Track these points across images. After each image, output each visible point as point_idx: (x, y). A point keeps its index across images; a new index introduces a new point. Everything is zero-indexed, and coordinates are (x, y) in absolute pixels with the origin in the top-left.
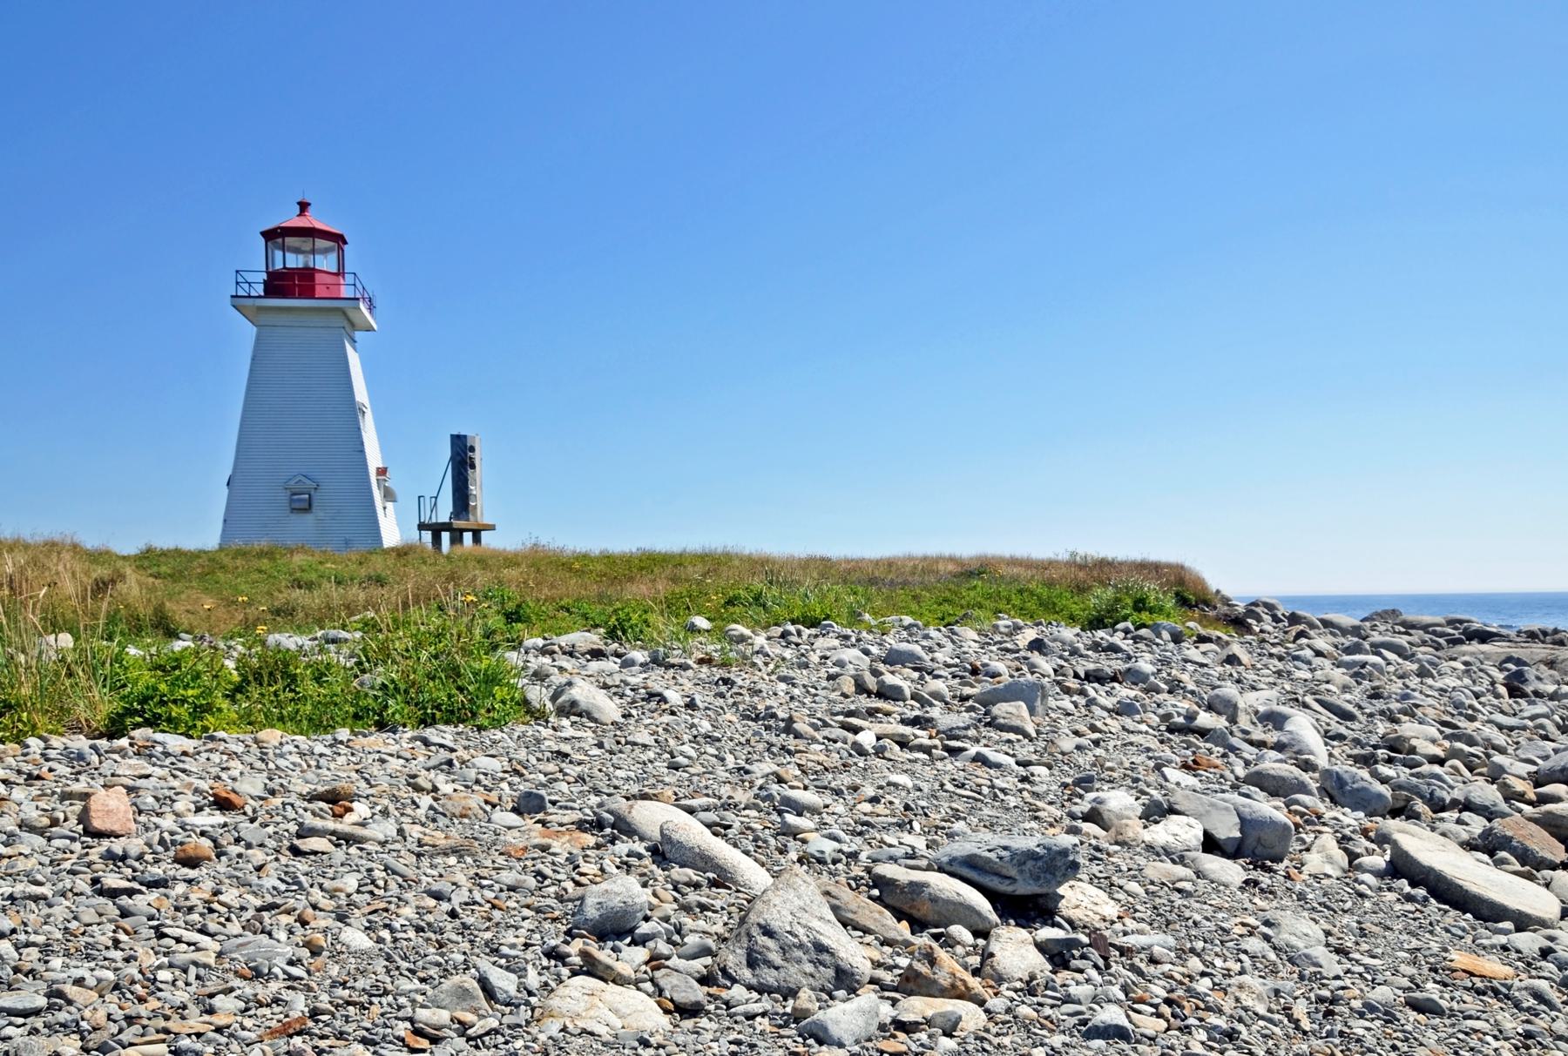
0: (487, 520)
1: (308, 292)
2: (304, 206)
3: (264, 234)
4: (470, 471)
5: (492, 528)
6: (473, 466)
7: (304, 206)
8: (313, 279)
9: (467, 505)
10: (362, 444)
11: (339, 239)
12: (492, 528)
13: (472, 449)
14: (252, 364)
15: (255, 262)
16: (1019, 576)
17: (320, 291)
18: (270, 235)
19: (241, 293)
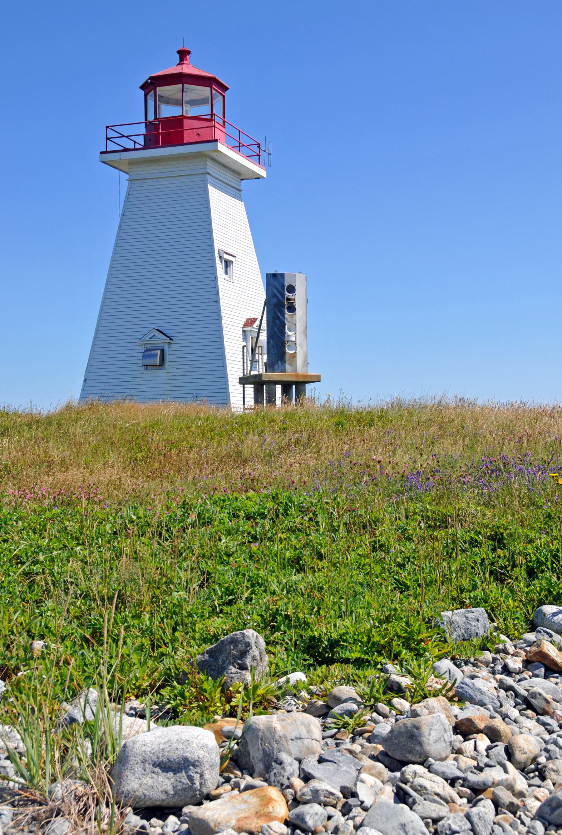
0: (312, 371)
1: (178, 141)
2: (183, 54)
3: (142, 88)
4: (287, 314)
5: (316, 379)
6: (292, 309)
7: (183, 54)
8: (182, 126)
9: (284, 353)
10: (218, 293)
11: (225, 88)
12: (316, 379)
13: (292, 289)
14: (121, 220)
15: (133, 114)
16: (103, 636)
17: (188, 136)
18: (151, 85)
19: (112, 147)
